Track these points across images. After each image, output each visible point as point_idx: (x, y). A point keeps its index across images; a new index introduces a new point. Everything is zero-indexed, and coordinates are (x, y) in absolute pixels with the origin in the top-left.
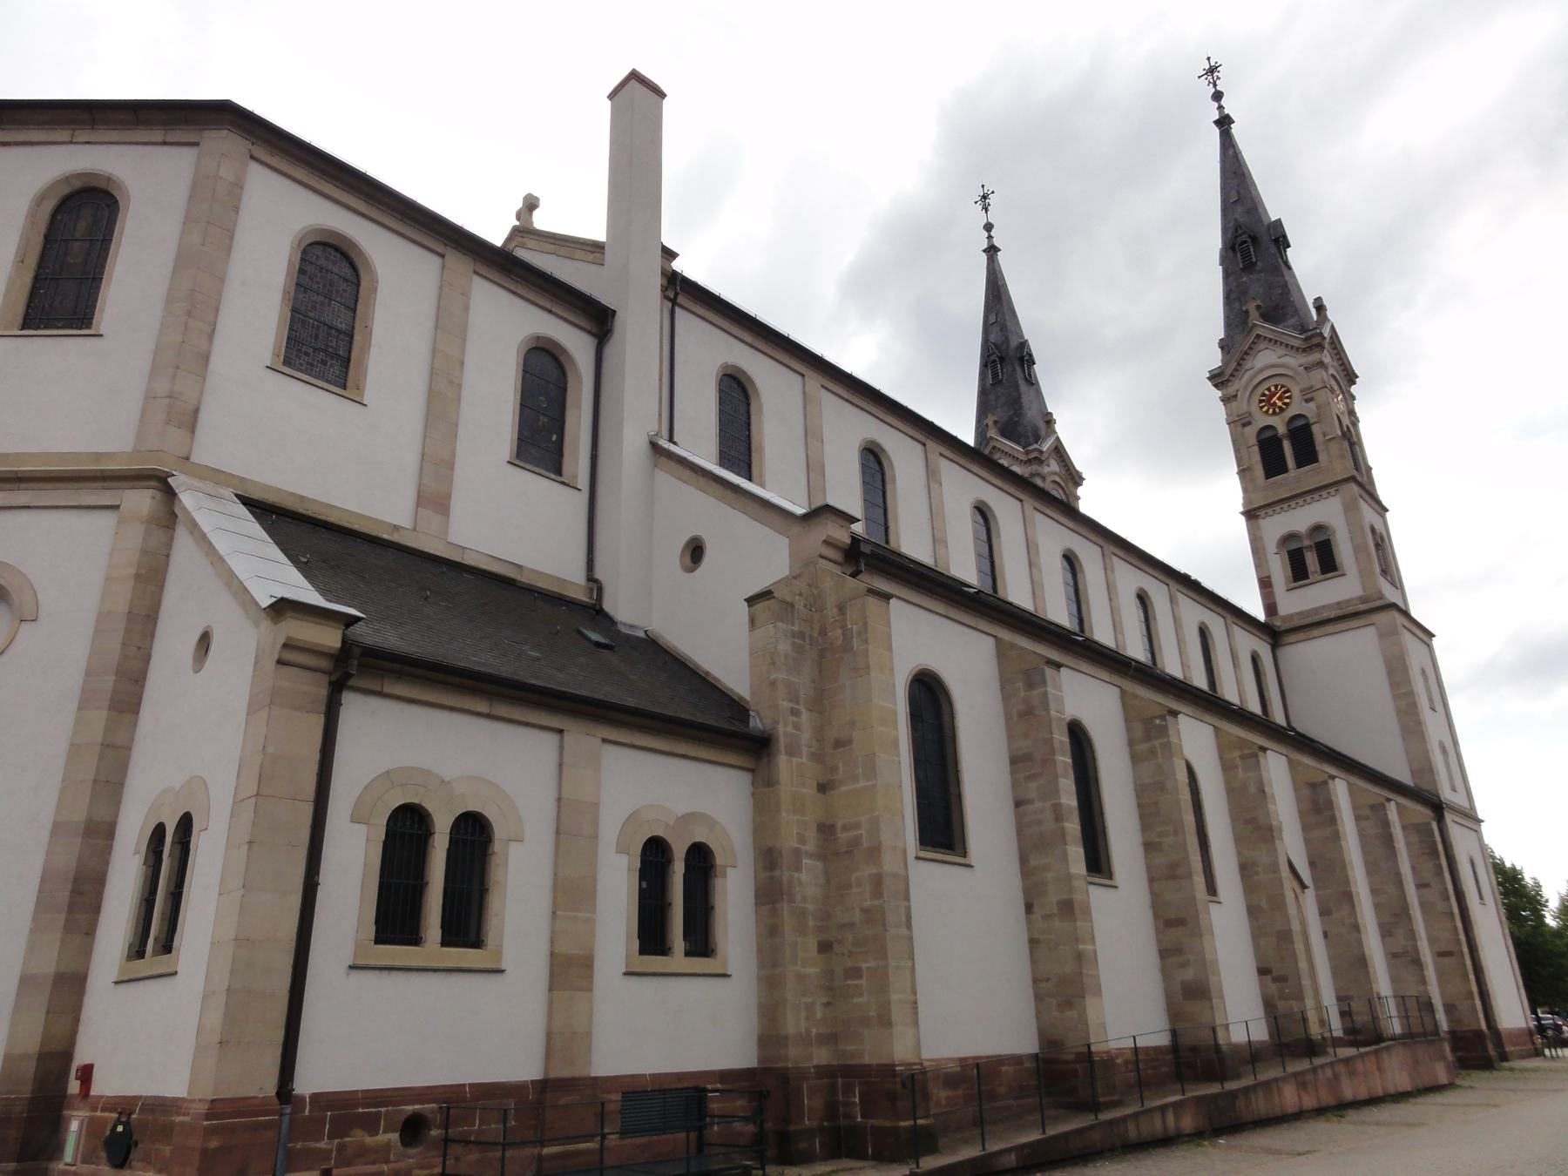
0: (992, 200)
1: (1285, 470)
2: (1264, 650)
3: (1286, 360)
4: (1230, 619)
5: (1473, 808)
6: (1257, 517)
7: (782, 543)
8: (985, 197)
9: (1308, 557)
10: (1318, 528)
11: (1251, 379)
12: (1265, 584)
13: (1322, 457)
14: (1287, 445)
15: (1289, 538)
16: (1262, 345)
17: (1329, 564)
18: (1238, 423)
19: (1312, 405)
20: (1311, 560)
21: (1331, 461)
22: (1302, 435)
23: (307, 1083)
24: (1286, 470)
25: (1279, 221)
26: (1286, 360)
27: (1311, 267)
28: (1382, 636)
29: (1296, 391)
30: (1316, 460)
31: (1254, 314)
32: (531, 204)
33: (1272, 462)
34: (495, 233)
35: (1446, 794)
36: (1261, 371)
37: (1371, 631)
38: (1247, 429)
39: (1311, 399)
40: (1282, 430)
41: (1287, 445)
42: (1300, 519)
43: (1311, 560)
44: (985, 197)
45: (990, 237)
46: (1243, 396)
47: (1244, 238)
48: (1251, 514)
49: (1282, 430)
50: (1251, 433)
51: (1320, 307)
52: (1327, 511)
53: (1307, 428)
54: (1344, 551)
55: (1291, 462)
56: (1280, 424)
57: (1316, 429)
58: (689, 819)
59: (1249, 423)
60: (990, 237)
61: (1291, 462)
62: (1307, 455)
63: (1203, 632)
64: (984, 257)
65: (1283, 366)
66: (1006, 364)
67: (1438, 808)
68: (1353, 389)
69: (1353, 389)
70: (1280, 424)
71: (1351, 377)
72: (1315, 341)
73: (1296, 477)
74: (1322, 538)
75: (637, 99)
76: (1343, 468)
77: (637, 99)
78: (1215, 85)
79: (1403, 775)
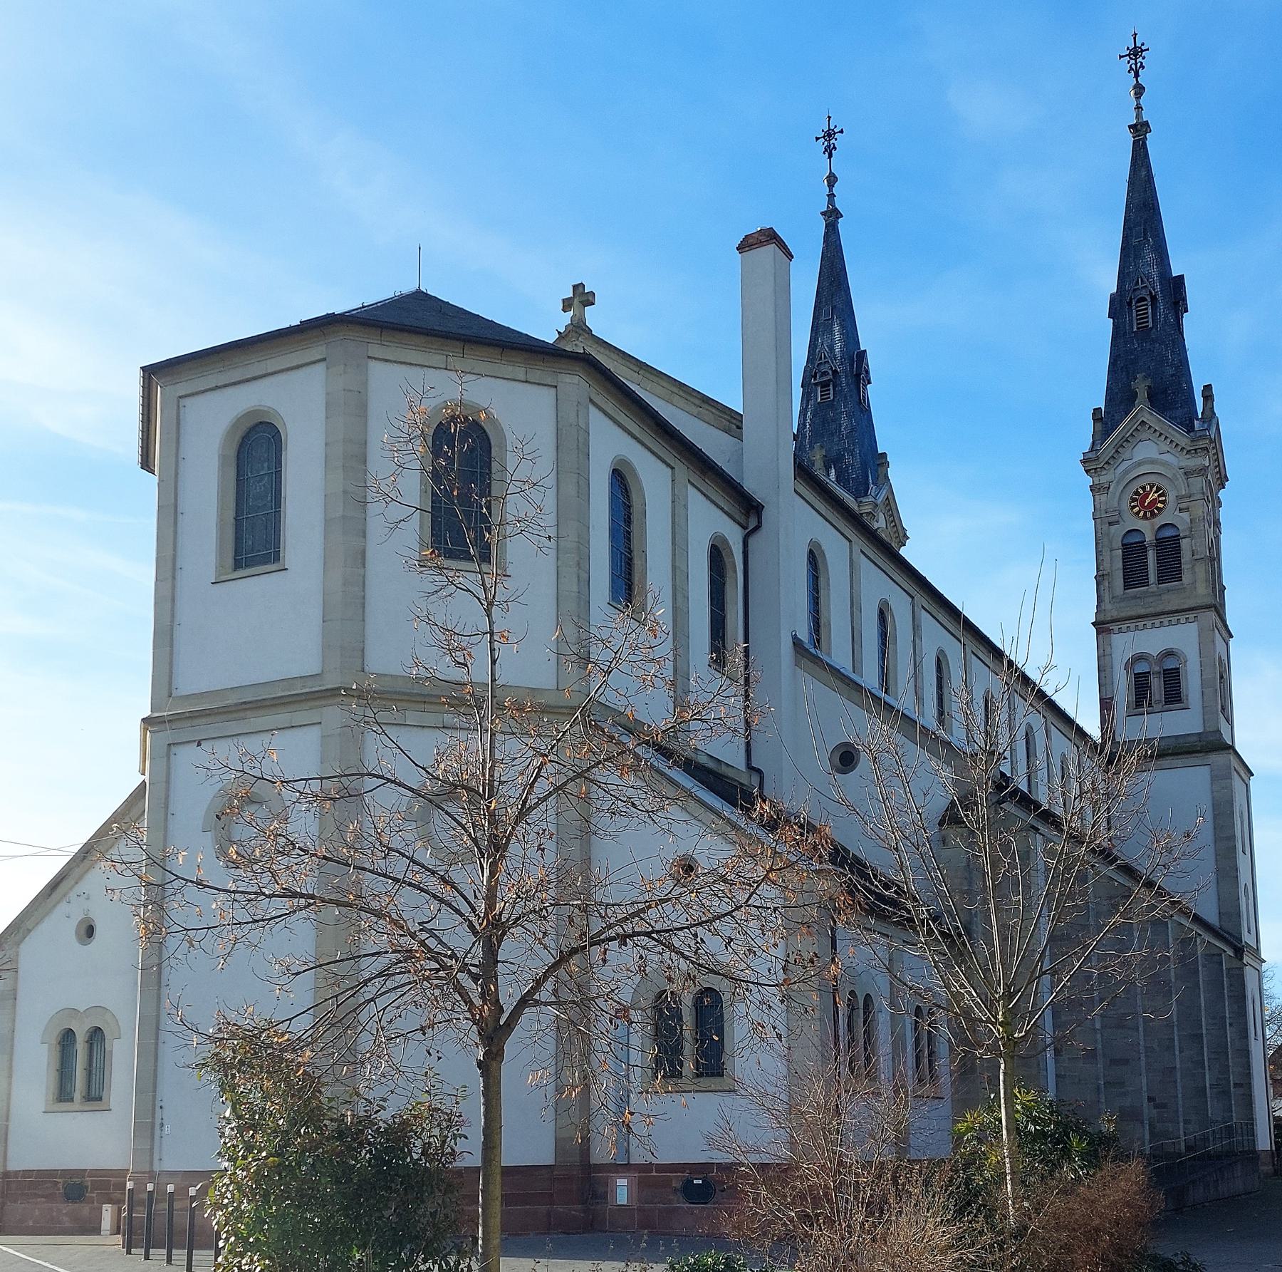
0: (839, 141)
1: (1145, 583)
2: (733, 535)
3: (1168, 458)
4: (683, 471)
5: (1258, 949)
6: (1109, 631)
7: (947, 773)
9: (1155, 685)
10: (1169, 653)
11: (1126, 472)
12: (1106, 704)
13: (1186, 578)
14: (1151, 555)
15: (1139, 658)
16: (1144, 436)
17: (1174, 696)
18: (1104, 520)
19: (1185, 515)
20: (1157, 685)
21: (1193, 574)
22: (1169, 547)
23: (509, 1157)
27: (1211, 342)
28: (1214, 778)
29: (1171, 497)
31: (1142, 394)
32: (581, 298)
33: (1134, 575)
34: (546, 325)
35: (1247, 938)
36: (1140, 464)
37: (1205, 771)
38: (1113, 528)
39: (1187, 509)
40: (1149, 537)
41: (1151, 555)
42: (1152, 641)
43: (1157, 685)
44: (829, 134)
45: (831, 196)
47: (1144, 293)
48: (1102, 626)
49: (1149, 537)
50: (1118, 532)
51: (1208, 392)
52: (1180, 637)
53: (1177, 538)
54: (1192, 684)
55: (1152, 577)
56: (1148, 529)
57: (1185, 543)
59: (1117, 522)
60: (831, 196)
61: (1152, 577)
62: (1171, 569)
63: (621, 480)
64: (1129, 139)
65: (1165, 464)
66: (839, 379)
67: (1239, 951)
68: (1222, 494)
69: (1222, 494)
70: (1148, 529)
71: (1222, 480)
72: (1203, 443)
73: (1155, 592)
74: (1170, 664)
76: (1202, 592)
78: (1137, 75)
79: (1212, 917)
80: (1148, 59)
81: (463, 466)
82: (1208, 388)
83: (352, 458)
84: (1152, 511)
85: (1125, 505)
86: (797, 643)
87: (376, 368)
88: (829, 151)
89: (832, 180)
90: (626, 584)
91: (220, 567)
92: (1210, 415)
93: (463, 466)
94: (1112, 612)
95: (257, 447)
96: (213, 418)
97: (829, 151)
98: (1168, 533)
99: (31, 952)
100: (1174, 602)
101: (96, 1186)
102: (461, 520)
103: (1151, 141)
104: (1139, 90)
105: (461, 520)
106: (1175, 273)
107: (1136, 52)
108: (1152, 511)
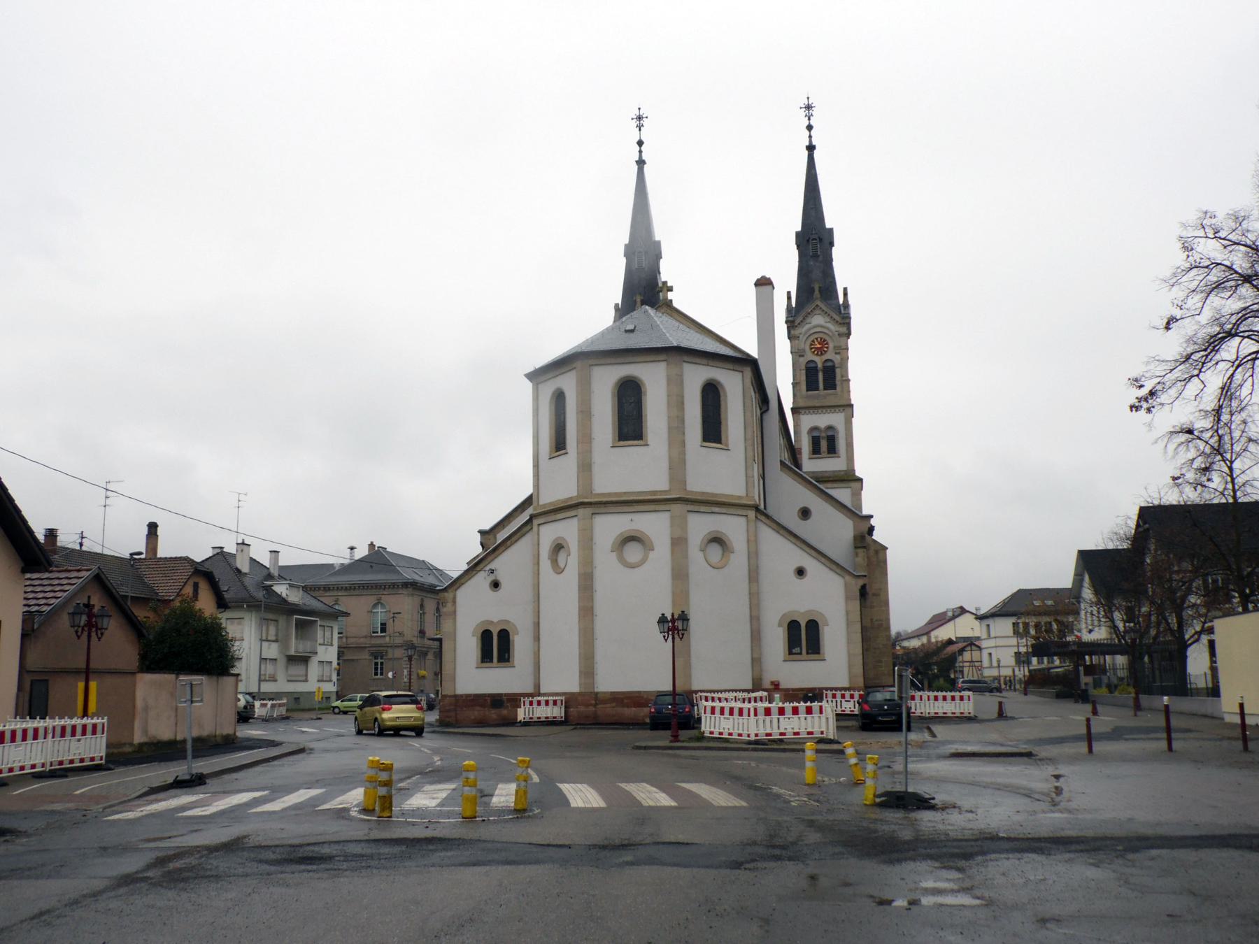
0: (645, 122)
1: (817, 389)
3: (829, 325)
8: (640, 118)
10: (830, 428)
13: (838, 388)
15: (815, 429)
16: (818, 311)
17: (832, 450)
19: (838, 357)
20: (824, 444)
24: (817, 389)
25: (831, 230)
26: (829, 325)
27: (846, 269)
29: (831, 345)
30: (835, 388)
33: (812, 385)
38: (801, 359)
40: (820, 366)
43: (824, 444)
44: (640, 118)
45: (640, 152)
46: (803, 338)
49: (820, 366)
50: (803, 361)
52: (835, 419)
53: (833, 368)
56: (819, 361)
57: (838, 371)
58: (500, 622)
64: (806, 153)
74: (830, 433)
75: (153, 527)
77: (153, 527)
80: (815, 112)
81: (629, 399)
82: (845, 289)
83: (676, 402)
84: (821, 351)
85: (807, 348)
86: (782, 463)
87: (685, 365)
88: (640, 127)
89: (640, 143)
90: (713, 431)
91: (614, 441)
92: (846, 305)
93: (629, 399)
94: (801, 403)
95: (559, 397)
96: (548, 390)
97: (640, 127)
98: (829, 364)
99: (463, 594)
100: (832, 401)
101: (509, 700)
102: (630, 426)
103: (816, 153)
104: (810, 128)
105: (630, 426)
106: (828, 226)
107: (809, 107)
108: (821, 351)
